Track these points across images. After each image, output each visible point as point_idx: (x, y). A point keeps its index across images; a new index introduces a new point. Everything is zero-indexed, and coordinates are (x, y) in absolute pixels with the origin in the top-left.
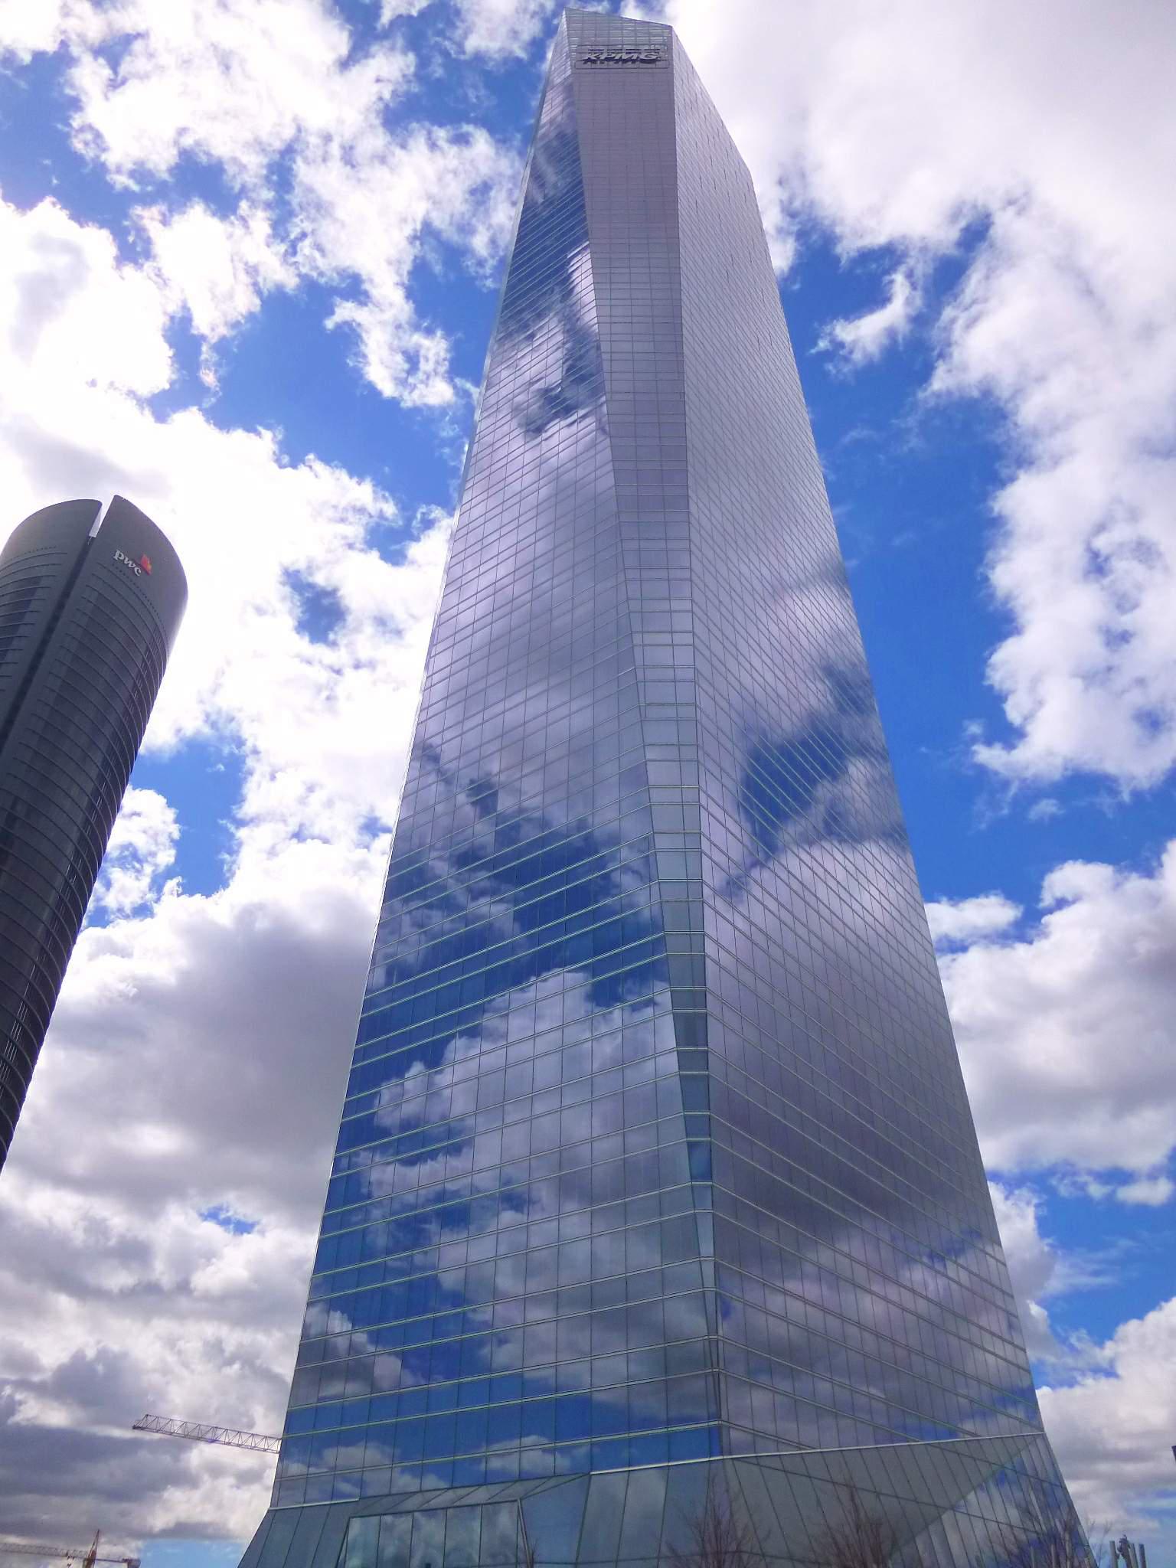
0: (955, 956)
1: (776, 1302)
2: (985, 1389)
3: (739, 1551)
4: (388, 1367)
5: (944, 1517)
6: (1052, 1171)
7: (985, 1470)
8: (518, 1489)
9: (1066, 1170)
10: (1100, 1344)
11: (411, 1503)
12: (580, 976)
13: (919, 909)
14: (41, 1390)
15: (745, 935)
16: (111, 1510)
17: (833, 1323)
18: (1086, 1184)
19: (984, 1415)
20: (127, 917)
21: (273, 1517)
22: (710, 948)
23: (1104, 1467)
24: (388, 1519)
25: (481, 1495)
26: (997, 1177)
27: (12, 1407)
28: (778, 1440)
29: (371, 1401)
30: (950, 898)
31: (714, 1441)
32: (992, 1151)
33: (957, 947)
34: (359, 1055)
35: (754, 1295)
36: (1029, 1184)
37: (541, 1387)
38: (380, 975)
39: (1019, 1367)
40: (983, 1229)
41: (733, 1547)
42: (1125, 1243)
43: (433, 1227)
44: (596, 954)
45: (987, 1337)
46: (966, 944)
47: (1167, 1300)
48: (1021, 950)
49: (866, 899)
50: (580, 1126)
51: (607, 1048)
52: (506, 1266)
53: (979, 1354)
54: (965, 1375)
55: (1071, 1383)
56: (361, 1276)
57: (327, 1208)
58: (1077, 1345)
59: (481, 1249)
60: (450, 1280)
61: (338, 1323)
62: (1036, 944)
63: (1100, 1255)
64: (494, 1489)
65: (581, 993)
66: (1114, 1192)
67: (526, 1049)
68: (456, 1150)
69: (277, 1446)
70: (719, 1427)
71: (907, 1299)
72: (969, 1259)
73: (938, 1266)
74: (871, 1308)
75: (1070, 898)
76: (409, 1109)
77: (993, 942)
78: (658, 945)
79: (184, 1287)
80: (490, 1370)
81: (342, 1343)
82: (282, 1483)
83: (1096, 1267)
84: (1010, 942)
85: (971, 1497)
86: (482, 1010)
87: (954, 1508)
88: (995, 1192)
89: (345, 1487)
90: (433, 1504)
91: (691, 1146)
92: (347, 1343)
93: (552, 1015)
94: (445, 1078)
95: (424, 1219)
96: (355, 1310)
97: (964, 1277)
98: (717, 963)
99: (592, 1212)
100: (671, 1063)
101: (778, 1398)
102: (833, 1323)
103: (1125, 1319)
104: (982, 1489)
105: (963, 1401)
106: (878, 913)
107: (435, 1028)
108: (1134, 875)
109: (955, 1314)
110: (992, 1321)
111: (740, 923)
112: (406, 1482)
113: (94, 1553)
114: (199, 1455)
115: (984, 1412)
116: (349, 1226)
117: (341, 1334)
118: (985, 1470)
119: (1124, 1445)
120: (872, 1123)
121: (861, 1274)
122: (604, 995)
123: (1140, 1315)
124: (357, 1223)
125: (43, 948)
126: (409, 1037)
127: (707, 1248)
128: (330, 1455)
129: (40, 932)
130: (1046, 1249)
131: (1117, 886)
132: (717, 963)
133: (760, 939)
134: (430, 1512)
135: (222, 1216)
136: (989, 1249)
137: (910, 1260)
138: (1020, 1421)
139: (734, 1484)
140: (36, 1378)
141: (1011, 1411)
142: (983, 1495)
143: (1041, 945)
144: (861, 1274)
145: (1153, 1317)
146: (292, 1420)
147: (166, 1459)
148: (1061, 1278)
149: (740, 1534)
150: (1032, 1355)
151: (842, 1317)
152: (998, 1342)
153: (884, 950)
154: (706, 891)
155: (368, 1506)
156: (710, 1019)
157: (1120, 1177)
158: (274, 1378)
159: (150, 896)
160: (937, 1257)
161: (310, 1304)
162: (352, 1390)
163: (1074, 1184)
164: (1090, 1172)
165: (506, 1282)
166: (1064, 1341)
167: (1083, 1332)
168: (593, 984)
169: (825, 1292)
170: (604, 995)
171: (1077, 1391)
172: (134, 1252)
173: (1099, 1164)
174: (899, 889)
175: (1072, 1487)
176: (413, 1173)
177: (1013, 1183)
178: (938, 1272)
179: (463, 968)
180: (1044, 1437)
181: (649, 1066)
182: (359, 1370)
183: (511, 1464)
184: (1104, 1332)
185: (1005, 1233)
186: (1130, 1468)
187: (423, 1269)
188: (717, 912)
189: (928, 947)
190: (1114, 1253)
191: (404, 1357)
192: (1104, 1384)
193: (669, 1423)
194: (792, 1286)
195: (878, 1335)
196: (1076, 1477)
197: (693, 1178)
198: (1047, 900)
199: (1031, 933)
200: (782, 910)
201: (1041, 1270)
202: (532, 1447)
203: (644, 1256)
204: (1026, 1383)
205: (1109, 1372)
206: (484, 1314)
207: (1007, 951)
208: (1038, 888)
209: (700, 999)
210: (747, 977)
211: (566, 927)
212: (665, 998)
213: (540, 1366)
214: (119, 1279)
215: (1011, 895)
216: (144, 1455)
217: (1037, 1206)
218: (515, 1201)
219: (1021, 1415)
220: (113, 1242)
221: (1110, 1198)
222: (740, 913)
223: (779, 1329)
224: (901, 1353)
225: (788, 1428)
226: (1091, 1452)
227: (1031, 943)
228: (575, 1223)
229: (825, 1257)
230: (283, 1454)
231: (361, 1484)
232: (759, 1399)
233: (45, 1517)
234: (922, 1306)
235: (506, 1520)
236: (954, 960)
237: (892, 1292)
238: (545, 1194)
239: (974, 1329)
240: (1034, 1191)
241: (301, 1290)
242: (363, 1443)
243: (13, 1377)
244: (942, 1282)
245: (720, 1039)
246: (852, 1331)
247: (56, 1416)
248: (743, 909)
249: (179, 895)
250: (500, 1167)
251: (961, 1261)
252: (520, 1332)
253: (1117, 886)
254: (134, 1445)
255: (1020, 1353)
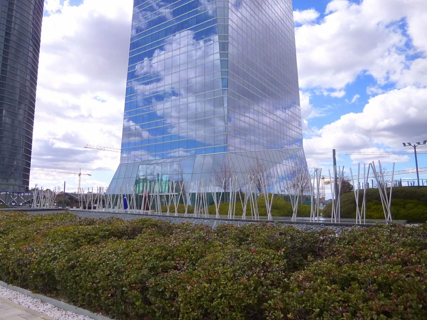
0: (298, 28)
1: (243, 118)
2: (291, 139)
3: (230, 171)
4: (145, 134)
5: (277, 165)
6: (315, 88)
7: (288, 155)
8: (178, 159)
9: (319, 88)
10: (319, 130)
11: (153, 162)
12: (190, 31)
13: (291, 12)
14: (59, 140)
15: (240, 19)
16: (82, 165)
17: (256, 123)
18: (323, 92)
19: (290, 145)
20: (54, 13)
21: (121, 165)
22: (230, 23)
23: (315, 156)
24: (148, 166)
25: (169, 160)
26: (301, 90)
27: (53, 144)
28: (241, 149)
29: (142, 141)
30: (299, 10)
31: (225, 149)
32: (302, 82)
33: (299, 25)
34: (131, 54)
35: (237, 116)
36: (309, 91)
37: (183, 137)
38: (134, 31)
39: (300, 134)
40: (296, 102)
41: (228, 170)
42: (329, 106)
43: (154, 100)
44: (197, 24)
45: (293, 127)
46: (302, 24)
47: (337, 120)
48: (317, 26)
49: (276, 8)
50: (192, 74)
51: (199, 53)
52: (173, 109)
53: (291, 131)
54: (287, 135)
55: (310, 138)
56: (136, 112)
57: (126, 95)
58: (314, 130)
59: (168, 105)
60: (159, 113)
61: (131, 123)
62: (322, 25)
63: (323, 109)
64: (172, 159)
65: (191, 36)
66: (330, 94)
67: (177, 52)
68: (158, 80)
69: (120, 151)
70: (227, 146)
71: (275, 118)
72: (292, 109)
73: (284, 110)
74: (267, 120)
75: (334, 11)
76: (145, 69)
77: (309, 24)
78: (215, 21)
79: (90, 116)
80: (171, 134)
81: (133, 128)
82: (122, 158)
83: (321, 112)
84: (314, 24)
85: (284, 161)
86: (163, 41)
87: (280, 163)
88: (300, 93)
89: (137, 159)
90: (158, 162)
91: (222, 78)
92: (134, 128)
93: (184, 42)
94: (155, 60)
95: (151, 98)
96: (135, 120)
97: (290, 113)
98: (232, 27)
99: (196, 96)
100: (218, 56)
101: (241, 140)
102: (256, 123)
103: (326, 124)
104: (287, 160)
105: (285, 141)
106: (279, 13)
107: (151, 46)
108: (354, 4)
109: (286, 122)
110: (296, 124)
111: (239, 14)
112: (151, 158)
113: (80, 173)
114: (101, 154)
115: (290, 144)
116: (132, 100)
117: (133, 125)
118: (288, 155)
119: (320, 151)
120: (271, 74)
121: (264, 112)
122: (197, 37)
123: (330, 123)
124: (134, 99)
125: (33, 23)
126: (145, 48)
127: (226, 105)
128: (133, 153)
129: (31, 18)
130: (310, 107)
131: (348, 7)
132: (232, 27)
133: (244, 20)
134: (157, 164)
135: (98, 99)
136: (297, 107)
137: (277, 109)
138: (298, 146)
139: (230, 158)
140: (57, 137)
141: (296, 144)
142: (287, 161)
143: (323, 25)
144: (264, 112)
145: (333, 124)
146: (123, 145)
147: (94, 155)
148: (314, 114)
149: (230, 167)
150: (303, 132)
151: (259, 122)
152: (296, 128)
153: (280, 25)
154: (230, 5)
155: (143, 162)
156: (229, 44)
157: (332, 90)
158: (117, 137)
159: (60, 6)
160: (284, 109)
161: (124, 119)
162: (137, 139)
163: (320, 92)
164: (325, 89)
165: (174, 114)
166: (310, 129)
167: (316, 127)
168: (195, 34)
169: (255, 116)
170: (197, 37)
171: (312, 140)
172: (76, 108)
173: (327, 87)
174: (286, 5)
175: (307, 160)
176: (148, 87)
177: (306, 91)
178: (283, 112)
179: (159, 28)
180: (303, 149)
181: (212, 57)
182: (139, 134)
183: (177, 154)
184: (320, 127)
185: (301, 103)
186: (320, 156)
187: (152, 110)
188: (232, 11)
189: (292, 24)
190: (326, 109)
191: (149, 131)
192: (319, 138)
193: (215, 145)
194: (247, 114)
195: (267, 126)
196: (308, 158)
197: (223, 87)
198: (327, 11)
199: (321, 21)
200: (252, 11)
201: (309, 112)
202: (181, 150)
203: (209, 107)
204: (301, 138)
205: (320, 136)
206: (169, 121)
207: (313, 27)
208: (325, 7)
209: (226, 38)
210: (240, 32)
211: (189, 15)
212: (216, 37)
213: (183, 134)
214: (73, 114)
215: (317, 10)
216: (88, 153)
217: (310, 97)
218: (174, 94)
219: (299, 144)
220: (70, 105)
221: (328, 96)
222: (239, 12)
223: (243, 124)
224: (272, 130)
225: (243, 147)
226: (312, 153)
227: (320, 24)
228: (191, 99)
229: (256, 108)
230: (122, 152)
231: (141, 159)
232: (237, 140)
233: (67, 166)
234: (278, 120)
235: (175, 166)
236: (297, 29)
237: (272, 116)
238: (183, 92)
239: (290, 125)
240: (310, 93)
241: (122, 117)
242: (141, 150)
243: (52, 137)
244: (284, 114)
245: (231, 49)
246: (261, 125)
247: (65, 145)
248: (240, 10)
249: (69, 6)
250: (172, 84)
251: (290, 109)
252: (177, 125)
253: (348, 7)
254: (85, 151)
255: (300, 131)
